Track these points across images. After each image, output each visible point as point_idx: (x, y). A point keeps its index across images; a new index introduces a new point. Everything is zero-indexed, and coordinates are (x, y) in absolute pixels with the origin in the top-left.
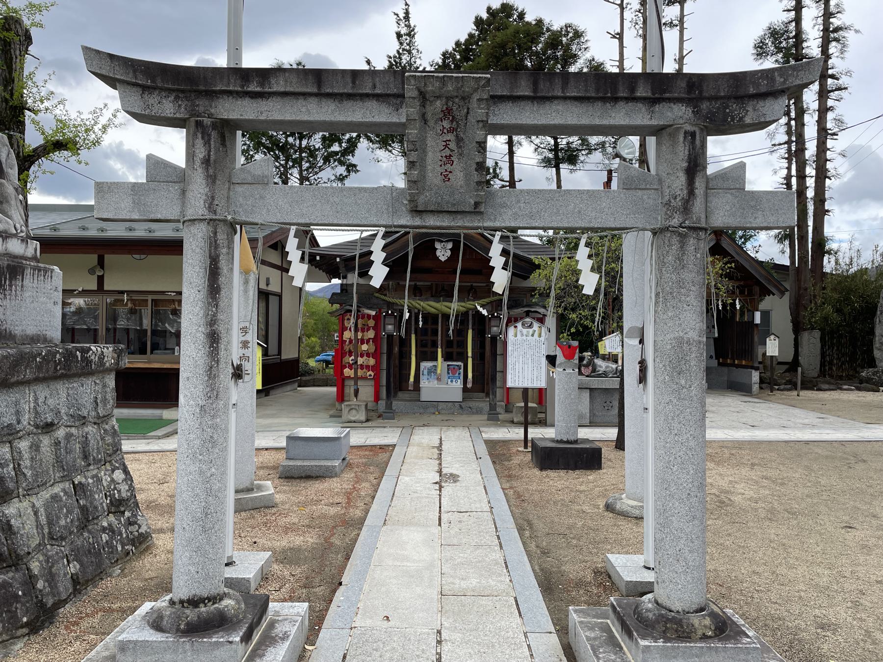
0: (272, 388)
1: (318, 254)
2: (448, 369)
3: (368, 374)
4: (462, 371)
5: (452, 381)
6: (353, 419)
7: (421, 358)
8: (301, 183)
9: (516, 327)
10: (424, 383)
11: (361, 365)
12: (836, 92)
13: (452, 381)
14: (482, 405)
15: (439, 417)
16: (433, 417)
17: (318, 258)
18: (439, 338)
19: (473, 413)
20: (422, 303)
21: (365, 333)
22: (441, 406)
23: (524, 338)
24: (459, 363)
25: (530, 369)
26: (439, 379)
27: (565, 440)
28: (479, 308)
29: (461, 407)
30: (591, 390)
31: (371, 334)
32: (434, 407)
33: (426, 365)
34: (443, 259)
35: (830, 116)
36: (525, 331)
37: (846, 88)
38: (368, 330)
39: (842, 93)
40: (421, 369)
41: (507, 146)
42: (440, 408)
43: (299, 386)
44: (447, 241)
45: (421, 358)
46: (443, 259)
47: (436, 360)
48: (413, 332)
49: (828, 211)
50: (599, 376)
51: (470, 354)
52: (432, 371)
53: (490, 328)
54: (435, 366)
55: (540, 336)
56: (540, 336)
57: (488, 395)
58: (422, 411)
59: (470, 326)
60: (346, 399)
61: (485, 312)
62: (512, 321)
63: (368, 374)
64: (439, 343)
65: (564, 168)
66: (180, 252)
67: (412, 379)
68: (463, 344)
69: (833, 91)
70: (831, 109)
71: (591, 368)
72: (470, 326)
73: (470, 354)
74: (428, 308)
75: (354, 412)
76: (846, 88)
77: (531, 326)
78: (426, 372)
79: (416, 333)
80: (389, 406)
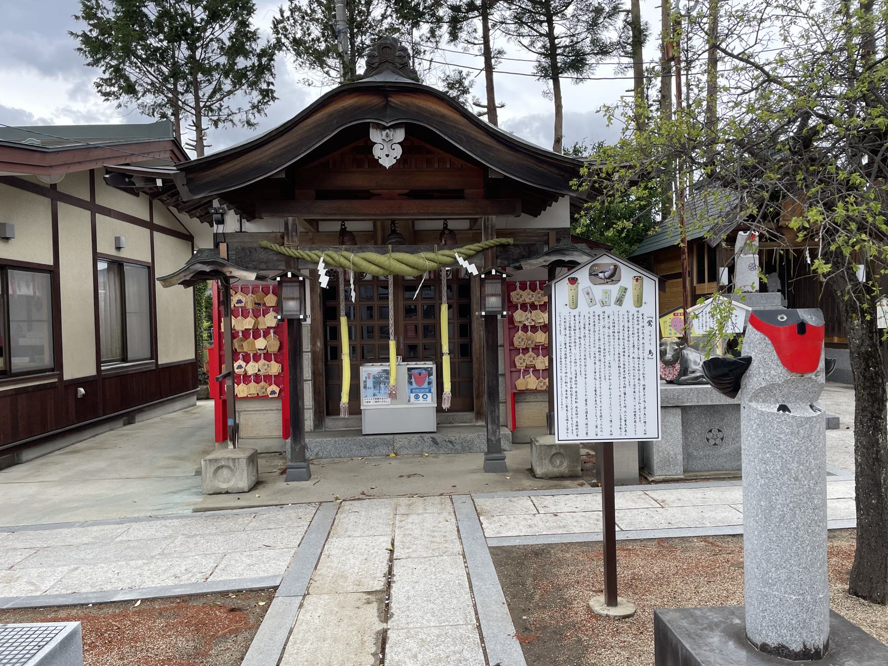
0: (141, 411)
1: (160, 175)
2: (410, 377)
3: (270, 389)
4: (433, 378)
5: (417, 397)
6: (224, 486)
7: (360, 357)
8: (216, 127)
9: (573, 281)
10: (368, 402)
11: (256, 375)
13: (417, 397)
14: (470, 435)
15: (394, 466)
16: (385, 464)
17: (159, 183)
18: (391, 322)
19: (457, 452)
20: (352, 256)
21: (261, 318)
22: (400, 441)
23: (598, 309)
24: (430, 365)
25: (616, 392)
26: (393, 396)
27: (796, 647)
28: (461, 261)
29: (434, 441)
30: (684, 409)
32: (391, 444)
33: (369, 371)
36: (598, 291)
40: (363, 378)
41: (483, 59)
42: (397, 446)
43: (198, 399)
44: (394, 127)
45: (360, 357)
47: (387, 360)
48: (343, 312)
51: (445, 348)
52: (380, 381)
53: (482, 298)
54: (387, 372)
55: (639, 302)
56: (639, 302)
57: (479, 415)
58: (365, 452)
59: (444, 299)
61: (473, 269)
62: (361, 365)
63: (270, 389)
64: (392, 330)
65: (565, 81)
66: (739, 410)
67: (345, 398)
68: (433, 331)
71: (678, 366)
72: (444, 299)
73: (445, 348)
75: (225, 472)
77: (613, 277)
78: (370, 384)
79: (348, 315)
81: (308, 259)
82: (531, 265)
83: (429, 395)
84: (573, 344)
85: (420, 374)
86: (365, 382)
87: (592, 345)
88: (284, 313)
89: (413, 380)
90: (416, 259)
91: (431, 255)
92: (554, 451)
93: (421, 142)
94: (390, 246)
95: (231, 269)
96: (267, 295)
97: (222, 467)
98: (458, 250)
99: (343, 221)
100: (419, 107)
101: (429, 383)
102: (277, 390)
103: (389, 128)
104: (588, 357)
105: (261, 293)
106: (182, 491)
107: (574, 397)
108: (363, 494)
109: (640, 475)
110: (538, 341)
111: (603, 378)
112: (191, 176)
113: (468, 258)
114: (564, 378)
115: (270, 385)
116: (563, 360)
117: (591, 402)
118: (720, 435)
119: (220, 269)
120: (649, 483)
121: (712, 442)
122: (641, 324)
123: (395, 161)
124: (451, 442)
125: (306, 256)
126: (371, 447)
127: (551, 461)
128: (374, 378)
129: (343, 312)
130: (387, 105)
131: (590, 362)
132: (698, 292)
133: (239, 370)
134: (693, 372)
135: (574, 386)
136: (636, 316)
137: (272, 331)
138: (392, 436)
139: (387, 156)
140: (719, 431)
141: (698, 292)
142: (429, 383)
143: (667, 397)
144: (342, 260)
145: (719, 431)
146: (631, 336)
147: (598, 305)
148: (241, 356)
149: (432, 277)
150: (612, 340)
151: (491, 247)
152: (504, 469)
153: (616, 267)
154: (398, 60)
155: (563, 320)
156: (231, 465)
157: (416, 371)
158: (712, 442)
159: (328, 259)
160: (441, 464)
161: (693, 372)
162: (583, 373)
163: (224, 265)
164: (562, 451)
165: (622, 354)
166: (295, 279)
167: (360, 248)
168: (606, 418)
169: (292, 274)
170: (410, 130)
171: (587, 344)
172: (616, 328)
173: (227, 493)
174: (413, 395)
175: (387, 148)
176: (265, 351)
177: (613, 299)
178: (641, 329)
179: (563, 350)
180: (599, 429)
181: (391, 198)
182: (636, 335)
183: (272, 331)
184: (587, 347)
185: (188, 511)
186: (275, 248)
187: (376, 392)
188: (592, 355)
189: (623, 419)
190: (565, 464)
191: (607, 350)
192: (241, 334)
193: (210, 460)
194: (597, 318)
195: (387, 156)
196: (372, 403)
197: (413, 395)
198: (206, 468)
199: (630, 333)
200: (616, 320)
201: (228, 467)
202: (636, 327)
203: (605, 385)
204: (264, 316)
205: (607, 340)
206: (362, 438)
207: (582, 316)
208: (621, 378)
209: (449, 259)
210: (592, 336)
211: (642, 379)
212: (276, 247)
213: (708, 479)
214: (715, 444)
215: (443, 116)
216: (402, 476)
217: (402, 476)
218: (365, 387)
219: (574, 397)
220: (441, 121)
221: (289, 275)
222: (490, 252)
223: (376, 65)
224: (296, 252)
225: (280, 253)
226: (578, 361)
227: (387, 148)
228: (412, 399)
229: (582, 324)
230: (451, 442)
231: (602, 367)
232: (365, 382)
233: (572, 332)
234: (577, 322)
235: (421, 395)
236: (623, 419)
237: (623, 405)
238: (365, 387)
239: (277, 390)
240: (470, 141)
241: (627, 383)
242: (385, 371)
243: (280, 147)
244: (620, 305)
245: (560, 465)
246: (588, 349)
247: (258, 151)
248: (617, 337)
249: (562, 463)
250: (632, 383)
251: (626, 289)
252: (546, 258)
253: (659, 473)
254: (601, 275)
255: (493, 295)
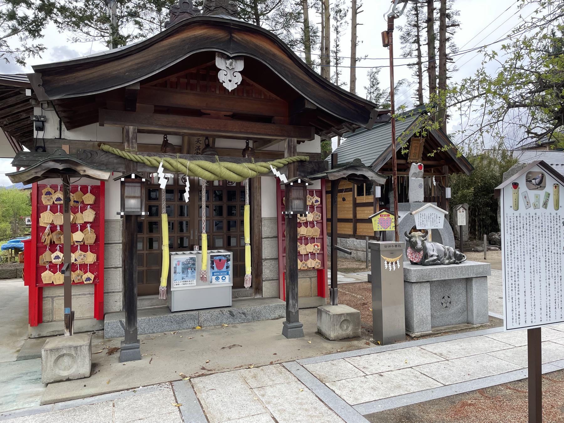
2: (212, 263)
3: (85, 276)
5: (217, 279)
6: (65, 374)
10: (178, 285)
12: (451, 28)
13: (217, 279)
19: (249, 321)
20: (188, 163)
25: (544, 284)
29: (232, 314)
31: (89, 216)
32: (193, 318)
33: (182, 257)
34: (230, 87)
35: (448, 44)
36: (532, 194)
37: (458, 25)
38: (83, 209)
39: (456, 29)
42: (201, 319)
44: (236, 58)
46: (230, 87)
48: (164, 210)
49: (448, 116)
50: (434, 263)
52: (190, 266)
58: (175, 326)
60: (45, 318)
63: (85, 276)
69: (449, 26)
70: (448, 39)
71: (422, 252)
74: (199, 170)
76: (458, 25)
78: (179, 269)
80: (131, 335)
81: (148, 163)
82: (335, 176)
83: (227, 277)
84: (516, 242)
85: (220, 260)
86: (175, 268)
87: (529, 243)
88: (126, 210)
89: (215, 265)
90: (241, 168)
91: (252, 166)
92: (343, 318)
93: (254, 71)
94: (217, 157)
95: (85, 168)
96: (85, 194)
97: (63, 355)
98: (271, 162)
99: (166, 134)
100: (256, 46)
101: (227, 267)
102: (92, 276)
103: (232, 58)
104: (526, 253)
105: (79, 192)
106: (13, 379)
107: (517, 289)
108: (203, 369)
109: (407, 334)
110: (302, 233)
111: (536, 272)
112: (47, 78)
113: (278, 169)
114: (510, 272)
115: (85, 273)
116: (509, 256)
117: (528, 293)
118: (449, 300)
119: (73, 167)
120: (412, 338)
121: (445, 305)
122: (559, 225)
123: (236, 86)
124: (244, 314)
125: (146, 161)
126: (180, 322)
127: (341, 327)
128: (183, 264)
129: (164, 210)
130: (231, 39)
131: (527, 257)
132: (358, 201)
133: (57, 260)
134: (432, 256)
135: (517, 280)
136: (555, 217)
137: (89, 225)
138: (197, 312)
139: (230, 81)
140: (449, 297)
141: (358, 201)
142: (227, 267)
143: (422, 275)
144: (179, 166)
145: (449, 297)
146: (553, 234)
147: (532, 207)
148: (58, 248)
149: (221, 184)
150: (541, 238)
151: (294, 162)
152: (301, 335)
153: (543, 176)
154: (229, 7)
155: (509, 221)
156: (73, 352)
157: (218, 258)
158: (445, 305)
159: (167, 164)
160: (242, 333)
161: (432, 256)
162: (523, 267)
163: (77, 164)
164: (348, 318)
165: (547, 250)
166: (137, 180)
167: (192, 157)
168: (538, 307)
169: (136, 176)
170: (249, 62)
171: (525, 242)
172: (544, 228)
173: (68, 380)
174: (214, 277)
175: (230, 75)
176: (82, 243)
177: (541, 203)
178: (558, 228)
179: (509, 247)
180: (533, 317)
181: (218, 118)
182: (556, 233)
183: (89, 225)
184: (525, 244)
185: (35, 405)
186: (116, 153)
187: (184, 276)
188: (529, 252)
189: (548, 307)
190: (350, 328)
191: (538, 247)
192: (58, 228)
193: (51, 350)
194: (531, 219)
195: (230, 81)
196: (180, 286)
197: (214, 277)
198: (47, 357)
199: (552, 232)
200: (543, 220)
201: (69, 355)
202: (556, 227)
203: (537, 276)
204: (82, 212)
205: (538, 239)
206: (172, 315)
207: (522, 217)
208: (547, 271)
209: (266, 170)
210: (528, 234)
211: (559, 271)
212: (117, 151)
213: (447, 332)
214: (446, 307)
215: (274, 55)
216: (223, 348)
217: (223, 348)
218: (175, 272)
219: (517, 289)
220: (273, 58)
221: (133, 176)
222: (292, 166)
223: (213, 8)
224: (136, 157)
225: (121, 157)
226: (519, 257)
227: (230, 75)
228: (214, 281)
229: (522, 224)
230: (244, 314)
231: (535, 261)
232: (175, 268)
233: (515, 231)
234: (519, 222)
235: (221, 277)
236: (548, 307)
237: (548, 294)
238: (175, 272)
239: (92, 276)
240: (293, 77)
241: (551, 276)
242: (191, 258)
243: (137, 61)
244: (546, 208)
245: (347, 329)
246: (526, 247)
247: (116, 63)
248: (544, 236)
249: (348, 327)
250: (554, 275)
251: (549, 194)
252: (345, 172)
253: (417, 330)
254: (533, 181)
255: (297, 199)
